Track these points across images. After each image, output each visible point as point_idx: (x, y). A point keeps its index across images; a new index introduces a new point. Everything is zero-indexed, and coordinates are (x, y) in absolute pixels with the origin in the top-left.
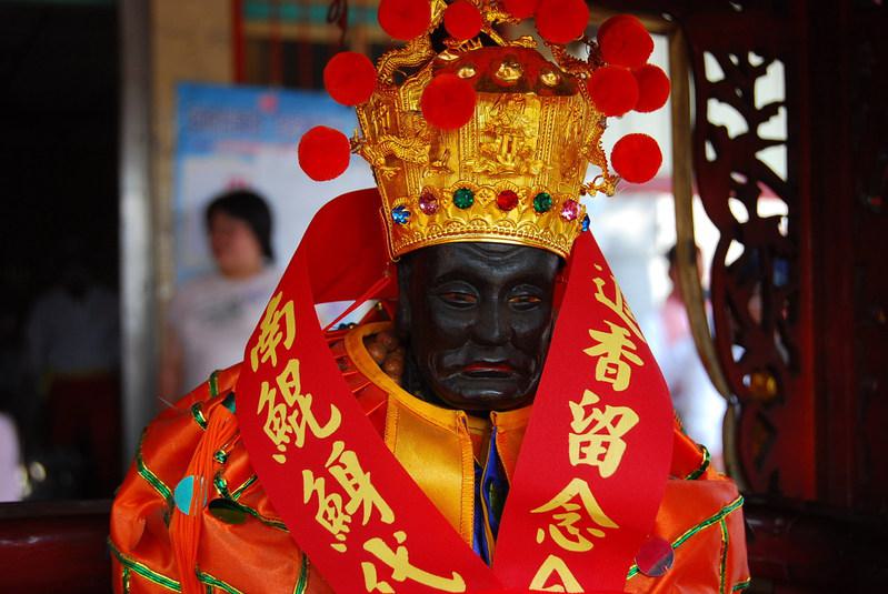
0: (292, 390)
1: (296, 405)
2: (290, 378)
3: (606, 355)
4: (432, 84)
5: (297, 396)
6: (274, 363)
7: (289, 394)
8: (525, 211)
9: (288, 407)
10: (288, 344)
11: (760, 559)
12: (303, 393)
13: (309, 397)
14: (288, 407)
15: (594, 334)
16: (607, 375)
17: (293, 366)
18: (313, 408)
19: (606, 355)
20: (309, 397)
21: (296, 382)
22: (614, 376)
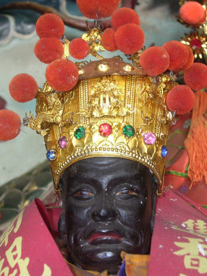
0: (15, 257)
1: (17, 266)
2: (15, 249)
3: (188, 254)
4: (70, 44)
5: (19, 260)
6: (6, 244)
7: (17, 248)
8: (133, 196)
9: (10, 268)
10: (16, 230)
11: (141, 169)
12: (23, 257)
13: (27, 260)
14: (10, 268)
15: (177, 244)
16: (192, 265)
17: (18, 242)
18: (29, 268)
19: (188, 254)
20: (27, 260)
21: (19, 251)
22: (197, 265)
